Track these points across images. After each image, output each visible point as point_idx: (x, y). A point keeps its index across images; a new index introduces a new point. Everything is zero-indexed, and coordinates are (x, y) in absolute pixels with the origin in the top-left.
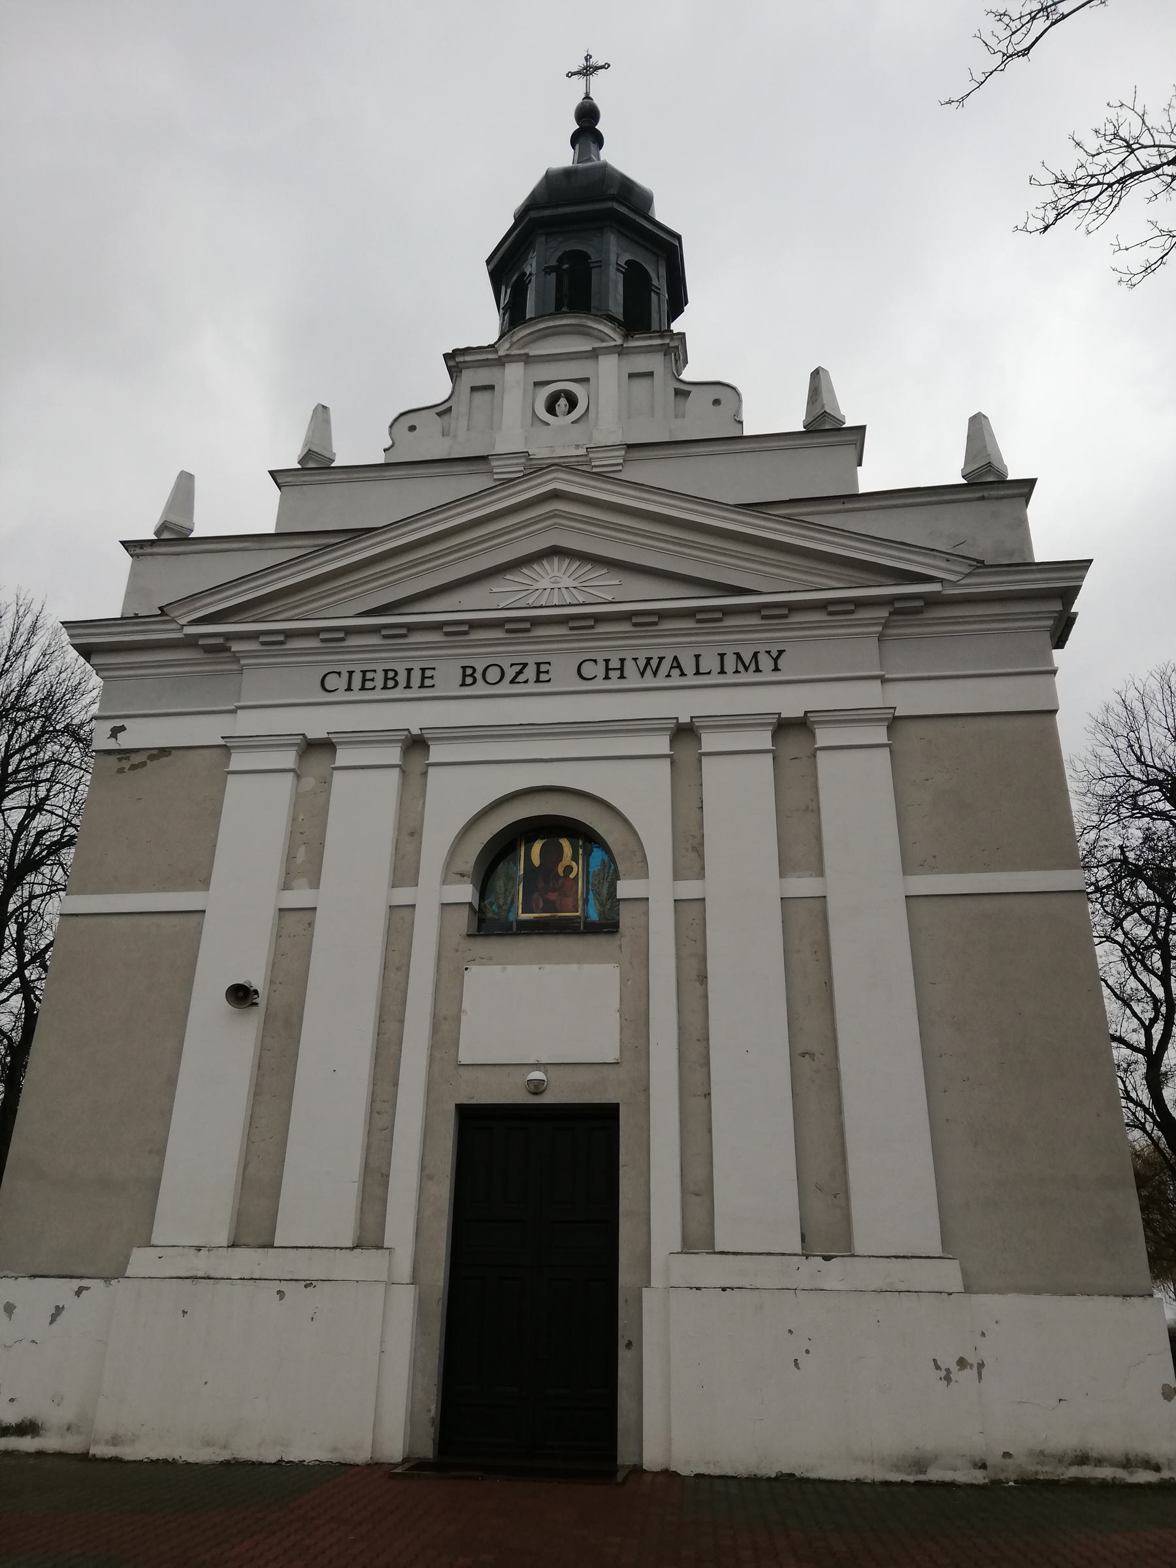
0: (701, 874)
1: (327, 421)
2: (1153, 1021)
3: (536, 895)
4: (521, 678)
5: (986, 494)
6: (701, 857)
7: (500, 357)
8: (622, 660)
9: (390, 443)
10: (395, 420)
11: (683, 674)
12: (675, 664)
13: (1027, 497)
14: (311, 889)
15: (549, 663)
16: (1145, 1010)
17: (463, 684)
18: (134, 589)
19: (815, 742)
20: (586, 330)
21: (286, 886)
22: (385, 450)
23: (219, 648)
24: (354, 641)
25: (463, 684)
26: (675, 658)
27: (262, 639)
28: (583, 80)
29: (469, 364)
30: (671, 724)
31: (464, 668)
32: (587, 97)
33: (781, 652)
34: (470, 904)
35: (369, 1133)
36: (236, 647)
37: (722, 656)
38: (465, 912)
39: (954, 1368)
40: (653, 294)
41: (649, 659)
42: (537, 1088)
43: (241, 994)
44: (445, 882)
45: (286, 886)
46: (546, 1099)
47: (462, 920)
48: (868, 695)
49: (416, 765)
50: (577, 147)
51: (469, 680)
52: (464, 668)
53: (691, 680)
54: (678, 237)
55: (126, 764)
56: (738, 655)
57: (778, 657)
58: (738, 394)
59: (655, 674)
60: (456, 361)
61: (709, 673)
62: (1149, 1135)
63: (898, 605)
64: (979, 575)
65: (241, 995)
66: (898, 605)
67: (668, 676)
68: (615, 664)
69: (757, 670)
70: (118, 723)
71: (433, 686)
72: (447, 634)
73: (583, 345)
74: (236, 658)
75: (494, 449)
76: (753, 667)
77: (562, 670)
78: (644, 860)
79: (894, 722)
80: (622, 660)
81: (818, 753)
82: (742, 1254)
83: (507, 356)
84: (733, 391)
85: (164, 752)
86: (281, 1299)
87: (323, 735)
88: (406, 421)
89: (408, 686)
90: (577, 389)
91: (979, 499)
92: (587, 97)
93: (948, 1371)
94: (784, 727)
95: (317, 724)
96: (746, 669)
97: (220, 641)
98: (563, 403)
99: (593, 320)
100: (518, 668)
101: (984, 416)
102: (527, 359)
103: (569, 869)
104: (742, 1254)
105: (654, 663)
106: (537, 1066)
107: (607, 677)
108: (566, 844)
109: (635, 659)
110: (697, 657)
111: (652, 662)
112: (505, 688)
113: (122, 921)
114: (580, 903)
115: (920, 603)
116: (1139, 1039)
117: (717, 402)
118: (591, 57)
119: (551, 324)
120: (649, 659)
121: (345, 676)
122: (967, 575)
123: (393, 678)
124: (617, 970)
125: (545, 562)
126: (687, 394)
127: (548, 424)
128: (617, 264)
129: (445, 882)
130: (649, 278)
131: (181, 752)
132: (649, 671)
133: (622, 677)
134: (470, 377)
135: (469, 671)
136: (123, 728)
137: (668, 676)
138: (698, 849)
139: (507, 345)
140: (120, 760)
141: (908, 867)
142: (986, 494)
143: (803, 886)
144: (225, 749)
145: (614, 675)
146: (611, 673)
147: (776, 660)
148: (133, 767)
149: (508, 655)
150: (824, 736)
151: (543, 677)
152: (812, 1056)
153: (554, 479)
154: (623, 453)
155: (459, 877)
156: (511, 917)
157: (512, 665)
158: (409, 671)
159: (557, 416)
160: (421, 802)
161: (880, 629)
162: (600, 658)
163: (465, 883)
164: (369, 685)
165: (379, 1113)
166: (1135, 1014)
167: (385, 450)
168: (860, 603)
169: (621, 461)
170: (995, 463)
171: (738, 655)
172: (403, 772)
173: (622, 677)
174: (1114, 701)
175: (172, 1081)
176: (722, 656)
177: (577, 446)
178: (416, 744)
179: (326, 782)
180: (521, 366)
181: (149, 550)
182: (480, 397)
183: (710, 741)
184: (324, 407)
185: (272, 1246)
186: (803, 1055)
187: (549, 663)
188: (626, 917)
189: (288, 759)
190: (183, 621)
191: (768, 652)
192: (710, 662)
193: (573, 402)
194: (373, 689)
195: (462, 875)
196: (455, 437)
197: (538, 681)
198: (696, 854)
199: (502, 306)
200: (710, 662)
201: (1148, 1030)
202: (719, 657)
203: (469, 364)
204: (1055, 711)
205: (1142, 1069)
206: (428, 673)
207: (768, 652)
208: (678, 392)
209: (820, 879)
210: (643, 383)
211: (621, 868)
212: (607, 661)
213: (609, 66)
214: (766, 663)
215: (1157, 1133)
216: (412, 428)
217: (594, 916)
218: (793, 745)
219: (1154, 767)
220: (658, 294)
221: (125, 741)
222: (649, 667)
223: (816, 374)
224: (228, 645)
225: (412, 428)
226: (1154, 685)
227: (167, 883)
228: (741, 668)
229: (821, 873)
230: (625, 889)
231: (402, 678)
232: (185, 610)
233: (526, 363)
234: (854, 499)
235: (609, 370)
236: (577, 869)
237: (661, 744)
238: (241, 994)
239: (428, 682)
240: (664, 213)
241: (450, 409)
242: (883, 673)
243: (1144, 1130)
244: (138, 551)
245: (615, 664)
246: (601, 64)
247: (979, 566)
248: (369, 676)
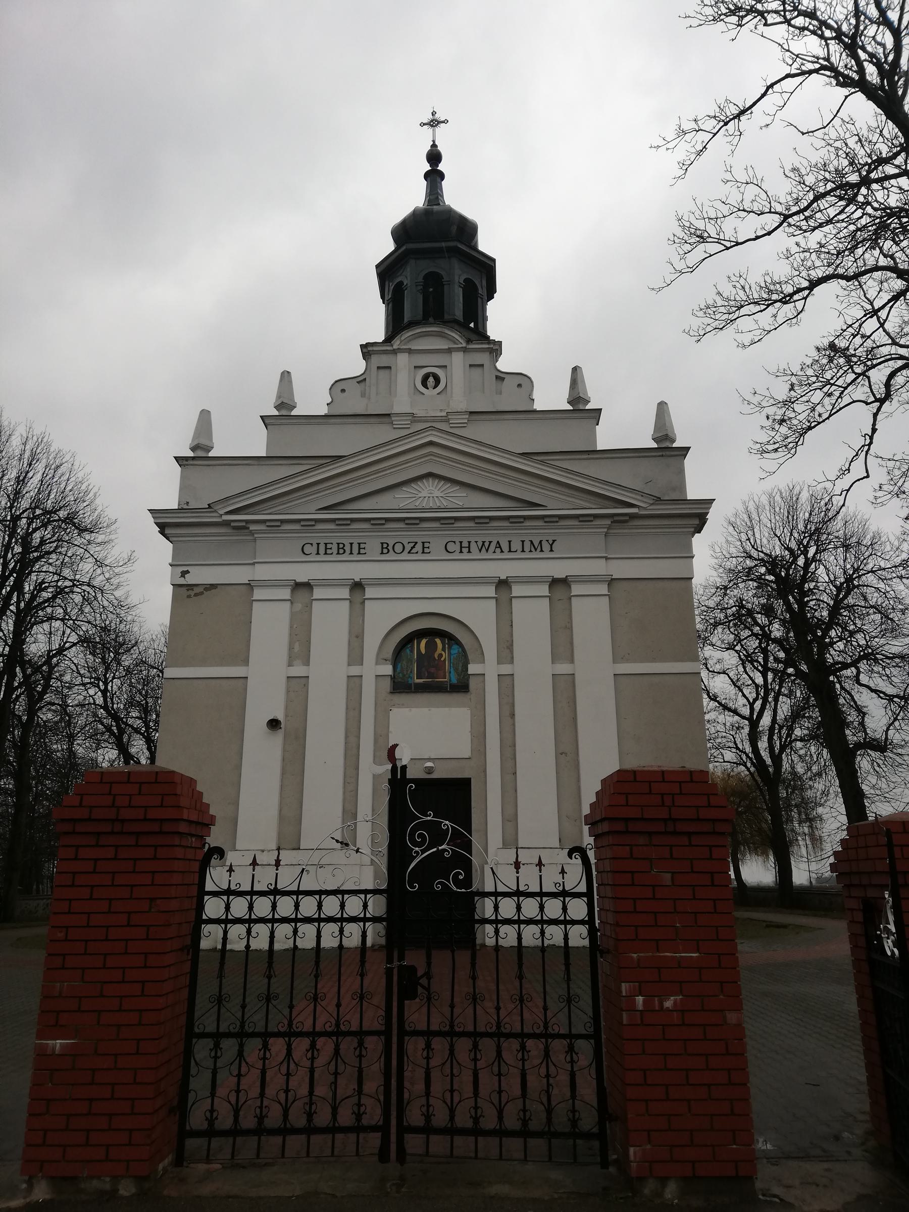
0: (511, 661)
1: (290, 382)
2: (755, 700)
4: (414, 551)
5: (664, 454)
6: (512, 652)
7: (394, 350)
8: (469, 542)
9: (331, 400)
10: (332, 385)
11: (502, 552)
12: (498, 546)
13: (685, 456)
14: (304, 665)
15: (429, 542)
16: (750, 692)
17: (382, 553)
18: (184, 487)
19: (571, 593)
20: (446, 335)
21: (290, 665)
22: (328, 404)
23: (243, 528)
24: (320, 526)
25: (382, 553)
26: (498, 542)
27: (268, 524)
28: (431, 130)
29: (376, 352)
30: (496, 580)
31: (382, 544)
32: (434, 145)
33: (554, 541)
34: (391, 675)
35: (344, 793)
36: (253, 527)
37: (523, 542)
38: (389, 680)
40: (479, 299)
41: (484, 542)
42: (429, 770)
43: (274, 724)
44: (377, 664)
45: (290, 665)
46: (434, 776)
47: (387, 684)
48: (598, 567)
49: (358, 598)
50: (429, 179)
51: (385, 551)
52: (382, 544)
53: (506, 555)
54: (494, 260)
55: (192, 593)
56: (531, 542)
57: (553, 543)
58: (532, 382)
59: (487, 550)
60: (367, 350)
61: (516, 551)
62: (748, 769)
63: (616, 518)
64: (658, 504)
65: (274, 724)
66: (616, 518)
67: (494, 552)
68: (465, 544)
69: (542, 551)
70: (185, 569)
71: (365, 553)
73: (443, 345)
74: (252, 533)
75: (392, 408)
76: (539, 549)
77: (437, 546)
78: (483, 654)
79: (612, 582)
80: (469, 542)
81: (572, 598)
82: (525, 848)
83: (399, 349)
84: (529, 379)
85: (213, 586)
86: (308, 874)
87: (305, 580)
88: (339, 386)
89: (351, 553)
90: (439, 372)
91: (659, 456)
92: (434, 145)
94: (555, 583)
95: (302, 573)
96: (536, 550)
97: (244, 524)
98: (431, 379)
99: (448, 329)
100: (412, 545)
101: (666, 403)
102: (410, 351)
103: (441, 656)
104: (525, 848)
105: (487, 544)
106: (429, 760)
107: (461, 552)
108: (438, 641)
109: (476, 542)
110: (510, 542)
111: (485, 543)
112: (405, 556)
113: (199, 681)
114: (447, 674)
115: (627, 518)
116: (746, 711)
117: (519, 385)
118: (436, 113)
119: (424, 330)
120: (484, 542)
121: (315, 546)
122: (652, 504)
123: (342, 548)
124: (469, 711)
125: (424, 481)
126: (503, 379)
127: (424, 394)
128: (459, 283)
129: (377, 664)
130: (477, 289)
131: (223, 587)
132: (484, 549)
133: (469, 552)
134: (376, 360)
135: (385, 546)
136: (188, 572)
137: (494, 552)
138: (510, 647)
139: (398, 342)
140: (188, 590)
141: (617, 658)
142: (664, 454)
143: (563, 668)
144: (250, 586)
145: (465, 550)
146: (463, 550)
147: (551, 545)
148: (196, 595)
149: (407, 537)
150: (576, 589)
151: (426, 550)
152: (566, 754)
153: (431, 434)
154: (467, 416)
155: (384, 661)
156: (410, 681)
157: (409, 543)
158: (351, 544)
159: (428, 389)
160: (361, 619)
161: (606, 530)
162: (457, 540)
163: (388, 664)
164: (329, 551)
165: (348, 783)
166: (744, 695)
167: (328, 404)
168: (596, 516)
169: (466, 421)
170: (670, 434)
171: (531, 542)
172: (350, 602)
173: (469, 552)
174: (741, 508)
175: (239, 767)
176: (523, 542)
177: (441, 410)
178: (357, 586)
179: (309, 606)
180: (407, 354)
181: (191, 462)
182: (382, 373)
183: (517, 590)
184: (288, 372)
185: (299, 849)
186: (562, 754)
187: (429, 542)
188: (472, 683)
189: (286, 593)
190: (222, 512)
191: (547, 541)
192: (516, 545)
193: (437, 380)
194: (332, 554)
195: (386, 660)
196: (369, 399)
197: (423, 552)
198: (508, 650)
199: (386, 298)
200: (516, 545)
201: (752, 705)
202: (521, 542)
203: (376, 352)
204: (692, 578)
205: (747, 730)
206: (362, 546)
207: (547, 541)
208: (497, 377)
209: (572, 665)
210: (479, 370)
211: (470, 657)
212: (461, 542)
213: (448, 122)
214: (546, 546)
215: (752, 769)
216: (343, 391)
217: (454, 681)
218: (560, 592)
219: (762, 552)
220: (482, 299)
221: (190, 579)
223: (575, 370)
224: (248, 526)
225: (343, 391)
226: (764, 500)
227: (223, 661)
228: (533, 549)
229: (572, 661)
230: (472, 669)
231: (347, 548)
232: (223, 506)
233: (409, 353)
234: (594, 453)
235: (458, 361)
236: (445, 655)
237: (491, 591)
238: (274, 724)
239: (362, 551)
240: (485, 244)
241: (365, 379)
242: (606, 555)
243: (745, 766)
244: (185, 463)
245: (465, 544)
246: (442, 119)
247: (658, 500)
248: (329, 546)
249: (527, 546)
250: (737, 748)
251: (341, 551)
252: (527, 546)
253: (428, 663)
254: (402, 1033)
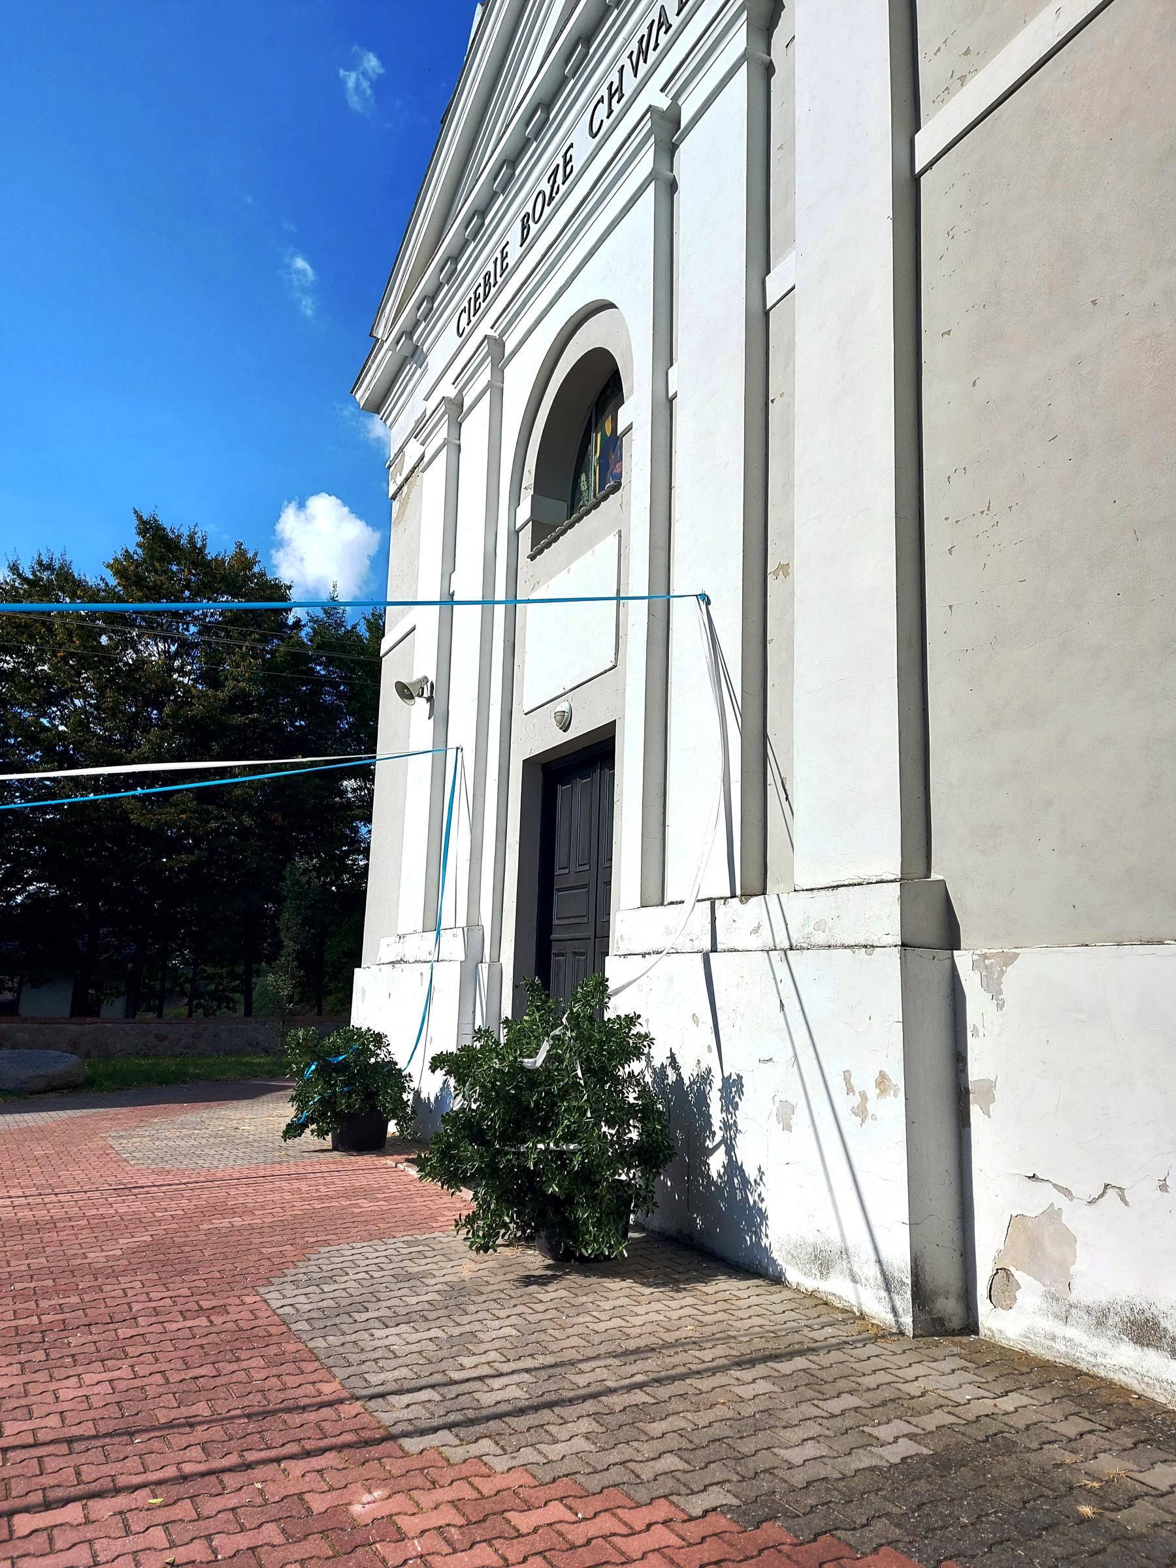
39: (872, 1092)
72: (557, 193)
93: (863, 1096)
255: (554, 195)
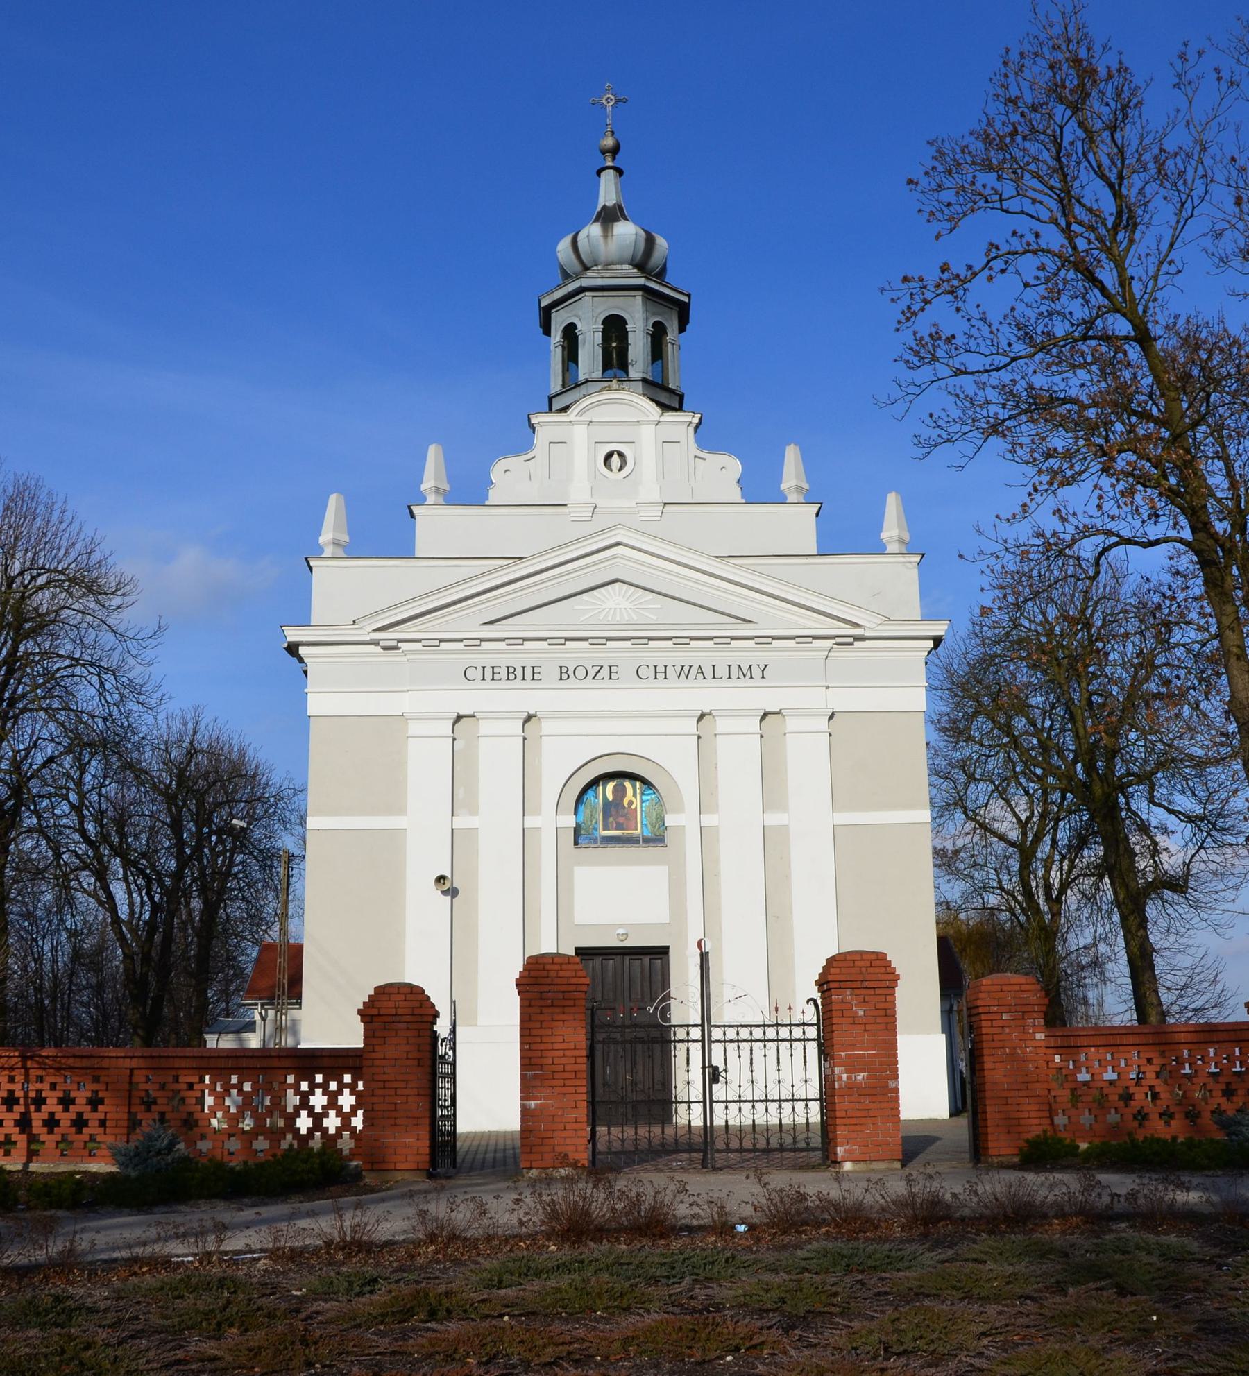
3: (611, 819)
68: (660, 669)
76: (748, 675)
87: (471, 713)
103: (631, 803)
105: (686, 669)
106: (621, 926)
116: (1014, 835)
143: (774, 819)
159: (611, 470)
214: (757, 672)
222: (685, 672)
231: (519, 673)
245: (660, 669)
249: (734, 670)
250: (1002, 889)
251: (512, 676)
252: (734, 670)
253: (613, 809)
254: (712, 1101)
255: (466, 642)
